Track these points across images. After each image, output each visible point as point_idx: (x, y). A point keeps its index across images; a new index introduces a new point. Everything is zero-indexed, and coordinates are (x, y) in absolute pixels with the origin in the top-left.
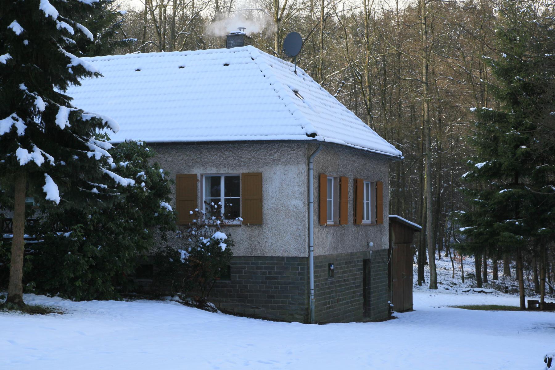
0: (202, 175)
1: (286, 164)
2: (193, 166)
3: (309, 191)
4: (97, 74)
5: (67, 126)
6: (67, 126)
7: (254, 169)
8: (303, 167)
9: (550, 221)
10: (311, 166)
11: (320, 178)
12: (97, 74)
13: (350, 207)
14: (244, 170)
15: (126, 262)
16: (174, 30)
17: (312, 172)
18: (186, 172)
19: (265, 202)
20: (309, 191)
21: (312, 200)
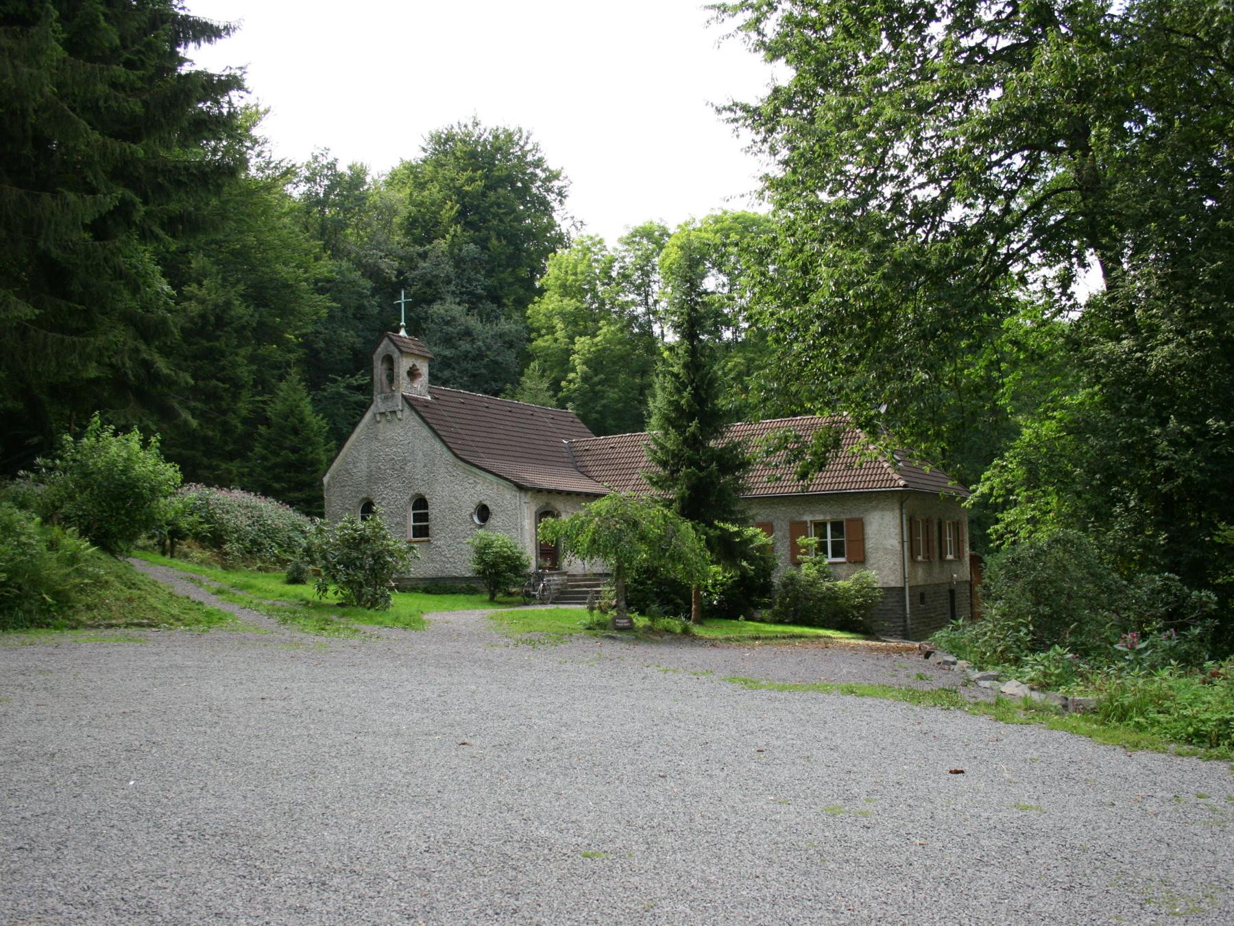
0: (811, 522)
1: (883, 509)
2: (804, 514)
3: (902, 532)
4: (707, 7)
5: (182, 61)
6: (182, 61)
7: (855, 515)
8: (897, 512)
9: (153, 439)
10: (904, 511)
11: (911, 520)
12: (707, 7)
13: (936, 544)
14: (848, 516)
15: (220, 154)
16: (744, 342)
17: (904, 516)
18: (797, 519)
19: (866, 541)
20: (902, 532)
21: (905, 539)
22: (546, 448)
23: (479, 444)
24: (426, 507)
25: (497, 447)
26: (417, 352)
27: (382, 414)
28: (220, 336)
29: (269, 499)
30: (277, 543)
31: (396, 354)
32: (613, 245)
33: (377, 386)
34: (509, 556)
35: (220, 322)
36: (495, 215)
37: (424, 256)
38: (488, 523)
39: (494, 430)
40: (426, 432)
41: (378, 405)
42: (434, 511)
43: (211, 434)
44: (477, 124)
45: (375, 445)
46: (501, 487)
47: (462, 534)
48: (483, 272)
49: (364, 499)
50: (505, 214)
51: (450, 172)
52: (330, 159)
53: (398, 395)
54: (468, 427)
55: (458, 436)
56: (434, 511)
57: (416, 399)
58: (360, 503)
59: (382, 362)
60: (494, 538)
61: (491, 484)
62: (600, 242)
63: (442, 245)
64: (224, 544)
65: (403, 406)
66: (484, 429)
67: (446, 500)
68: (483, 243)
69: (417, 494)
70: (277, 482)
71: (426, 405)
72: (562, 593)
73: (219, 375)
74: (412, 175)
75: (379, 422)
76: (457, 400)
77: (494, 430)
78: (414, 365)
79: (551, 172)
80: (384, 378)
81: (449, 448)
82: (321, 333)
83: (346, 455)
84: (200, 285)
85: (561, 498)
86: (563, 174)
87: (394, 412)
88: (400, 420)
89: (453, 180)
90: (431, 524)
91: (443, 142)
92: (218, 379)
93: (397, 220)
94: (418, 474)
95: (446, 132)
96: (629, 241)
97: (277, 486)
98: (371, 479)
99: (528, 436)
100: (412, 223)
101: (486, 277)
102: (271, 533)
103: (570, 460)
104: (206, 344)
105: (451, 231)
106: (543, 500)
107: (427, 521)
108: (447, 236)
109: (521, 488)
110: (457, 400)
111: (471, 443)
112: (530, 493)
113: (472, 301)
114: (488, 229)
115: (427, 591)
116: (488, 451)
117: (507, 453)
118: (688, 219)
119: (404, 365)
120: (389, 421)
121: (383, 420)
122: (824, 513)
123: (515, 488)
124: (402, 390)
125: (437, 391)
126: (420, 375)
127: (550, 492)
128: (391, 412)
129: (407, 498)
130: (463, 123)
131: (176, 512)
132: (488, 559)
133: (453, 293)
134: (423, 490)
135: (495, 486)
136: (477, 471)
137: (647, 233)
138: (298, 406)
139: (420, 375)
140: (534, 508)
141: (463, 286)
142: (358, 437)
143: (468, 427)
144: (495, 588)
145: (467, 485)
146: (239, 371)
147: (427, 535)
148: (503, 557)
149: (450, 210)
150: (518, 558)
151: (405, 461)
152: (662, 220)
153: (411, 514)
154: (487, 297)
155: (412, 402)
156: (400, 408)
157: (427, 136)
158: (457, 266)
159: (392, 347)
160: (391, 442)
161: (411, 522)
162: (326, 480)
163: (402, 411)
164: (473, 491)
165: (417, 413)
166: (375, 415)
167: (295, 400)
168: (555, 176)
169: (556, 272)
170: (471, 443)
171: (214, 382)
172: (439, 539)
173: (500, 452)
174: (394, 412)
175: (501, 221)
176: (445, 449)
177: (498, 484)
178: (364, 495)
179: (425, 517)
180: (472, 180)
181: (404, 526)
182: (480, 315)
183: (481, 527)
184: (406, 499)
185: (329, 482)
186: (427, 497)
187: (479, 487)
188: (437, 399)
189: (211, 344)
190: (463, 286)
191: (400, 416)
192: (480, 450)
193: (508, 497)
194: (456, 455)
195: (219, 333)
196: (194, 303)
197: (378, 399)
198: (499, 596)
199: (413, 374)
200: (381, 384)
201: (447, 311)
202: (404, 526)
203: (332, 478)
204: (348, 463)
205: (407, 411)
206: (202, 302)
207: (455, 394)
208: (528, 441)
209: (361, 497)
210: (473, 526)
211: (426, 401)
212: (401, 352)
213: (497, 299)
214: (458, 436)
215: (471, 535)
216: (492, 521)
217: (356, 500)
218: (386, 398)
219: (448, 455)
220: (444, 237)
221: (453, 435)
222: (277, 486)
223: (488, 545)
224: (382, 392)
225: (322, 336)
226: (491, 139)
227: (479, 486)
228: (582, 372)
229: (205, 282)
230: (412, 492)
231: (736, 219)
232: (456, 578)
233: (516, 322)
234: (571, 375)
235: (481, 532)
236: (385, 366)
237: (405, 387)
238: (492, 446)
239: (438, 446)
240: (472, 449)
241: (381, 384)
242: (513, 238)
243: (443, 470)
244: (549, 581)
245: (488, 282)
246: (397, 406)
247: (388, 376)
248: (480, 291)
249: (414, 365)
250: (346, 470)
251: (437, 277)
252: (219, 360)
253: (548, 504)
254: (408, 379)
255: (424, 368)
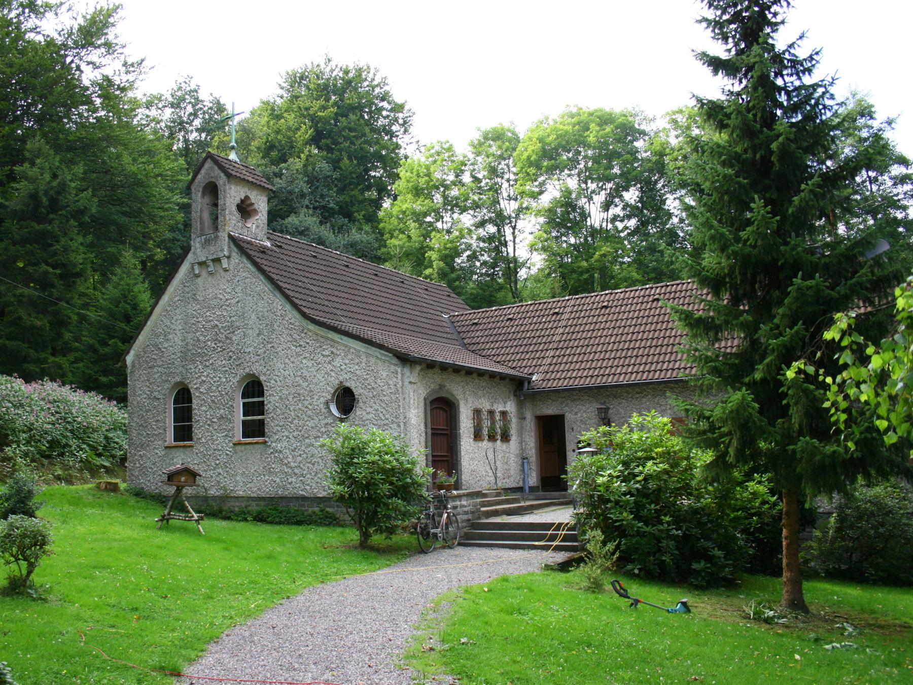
22: (424, 320)
23: (337, 306)
24: (261, 393)
25: (362, 311)
26: (250, 179)
27: (202, 264)
28: (53, 219)
29: (92, 394)
30: (89, 445)
31: (221, 180)
32: (463, 150)
33: (196, 225)
34: (393, 469)
35: (54, 205)
36: (346, 138)
37: (279, 175)
38: (352, 415)
39: (356, 292)
40: (261, 285)
41: (198, 252)
42: (272, 399)
43: (39, 323)
44: (329, 61)
45: (193, 308)
46: (373, 360)
47: (314, 433)
48: (335, 189)
49: (177, 384)
50: (356, 137)
51: (303, 103)
52: (193, 87)
53: (224, 236)
54: (322, 284)
55: (308, 292)
56: (272, 399)
57: (249, 243)
58: (173, 388)
59: (204, 194)
60: (365, 438)
61: (357, 354)
62: (449, 149)
63: (296, 163)
64: (8, 445)
65: (230, 251)
66: (343, 289)
67: (290, 383)
68: (336, 164)
69: (248, 375)
70: (105, 376)
71: (263, 250)
72: (474, 526)
73: (50, 261)
74: (273, 112)
75: (197, 276)
76: (308, 253)
77: (356, 292)
78: (247, 198)
79: (396, 104)
80: (206, 216)
81: (295, 306)
82: (178, 241)
83: (156, 325)
84: (33, 164)
85: (458, 379)
86: (407, 108)
87: (217, 260)
88: (226, 270)
89: (307, 109)
90: (267, 418)
91: (297, 80)
92: (48, 264)
93: (255, 144)
94: (250, 345)
95: (300, 71)
96: (478, 147)
97: (104, 379)
98: (189, 355)
99: (401, 304)
100: (270, 147)
101: (337, 193)
102: (82, 433)
103: (454, 337)
104: (38, 227)
105: (306, 152)
106: (436, 378)
107: (263, 414)
108: (302, 155)
109: (404, 359)
110: (308, 253)
111: (326, 303)
112: (418, 368)
113: (326, 215)
114: (340, 151)
115: (260, 518)
116: (350, 314)
117: (377, 320)
118: (541, 118)
119: (233, 195)
120: (211, 274)
121: (204, 273)
123: (395, 361)
124: (229, 228)
125: (279, 239)
126: (255, 212)
127: (444, 367)
128: (213, 260)
129: (235, 380)
130: (316, 64)
132: (360, 474)
133: (307, 207)
134: (256, 368)
135: (363, 357)
137: (497, 136)
138: (130, 291)
139: (255, 212)
140: (423, 393)
141: (316, 201)
142: (171, 299)
143: (322, 284)
144: (369, 525)
145: (321, 359)
146: (72, 257)
148: (384, 471)
149: (305, 132)
150: (409, 471)
151: (232, 329)
152: (512, 123)
153: (239, 403)
154: (339, 213)
155: (241, 243)
156: (226, 253)
157: (284, 74)
158: (310, 182)
159: (217, 171)
160: (214, 302)
161: (239, 416)
162: (129, 359)
163: (228, 257)
164: (329, 367)
165: (249, 257)
166: (193, 265)
167: (128, 285)
168: (398, 108)
169: (408, 174)
170: (326, 303)
171: (44, 267)
173: (366, 318)
174: (217, 260)
175: (352, 143)
176: (288, 307)
178: (178, 379)
179: (259, 408)
180: (324, 108)
181: (230, 421)
182: (333, 227)
183: (342, 420)
184: (233, 383)
186: (262, 378)
187: (338, 362)
188: (280, 247)
189: (42, 226)
190: (316, 201)
191: (225, 265)
192: (339, 312)
193: (385, 374)
194: (305, 315)
195: (51, 216)
196: (24, 183)
197: (196, 244)
198: (377, 539)
199: (245, 210)
200: (202, 223)
201: (301, 222)
202: (230, 421)
203: (138, 356)
204: (157, 336)
205: (236, 258)
206: (32, 180)
207: (307, 247)
208: (401, 309)
209: (173, 381)
210: (330, 420)
211: (265, 247)
212: (229, 176)
213: (349, 216)
214: (308, 292)
215: (328, 434)
216: (359, 412)
217: (167, 386)
218: (208, 242)
219: (293, 316)
220: (299, 157)
221: (300, 290)
222: (104, 379)
223: (357, 451)
224: (202, 235)
225: (179, 243)
226: (341, 75)
227: (338, 359)
228: (440, 269)
229: (38, 161)
230: (241, 372)
231: (591, 114)
232: (304, 498)
233: (367, 233)
234: (428, 271)
235: (343, 427)
236: (207, 200)
237: (232, 223)
238: (355, 310)
239: (279, 303)
240: (327, 309)
241: (202, 223)
242: (364, 160)
243: (285, 338)
244: (455, 508)
245: (341, 198)
246: (222, 250)
247: (212, 214)
248: (332, 205)
249: (247, 198)
251: (291, 193)
252: (51, 245)
253: (441, 387)
254: (238, 215)
255: (261, 204)
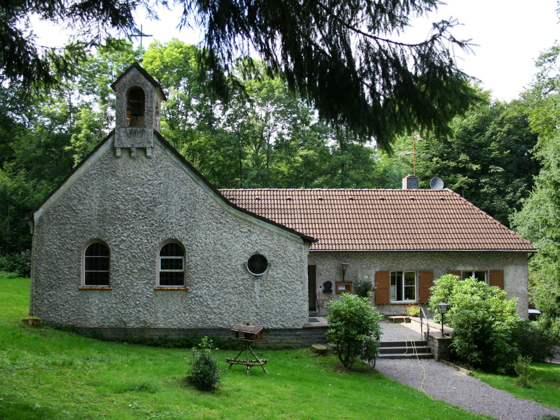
1: (516, 265)
2: (457, 265)
7: (497, 267)
18: (452, 269)
45: (111, 182)
46: (283, 239)
56: (193, 258)
75: (118, 158)
88: (149, 158)
98: (103, 218)
122: (473, 265)
131: (40, 108)
134: (178, 235)
136: (254, 220)
147: (107, 282)
151: (155, 203)
153: (158, 260)
160: (136, 181)
161: (158, 269)
164: (246, 240)
172: (200, 289)
177: (279, 235)
178: (95, 236)
185: (41, 219)
186: (184, 243)
187: (254, 237)
200: (361, 60)
203: (47, 213)
230: (163, 237)
232: (221, 329)
241: (361, 60)
250: (68, 207)
